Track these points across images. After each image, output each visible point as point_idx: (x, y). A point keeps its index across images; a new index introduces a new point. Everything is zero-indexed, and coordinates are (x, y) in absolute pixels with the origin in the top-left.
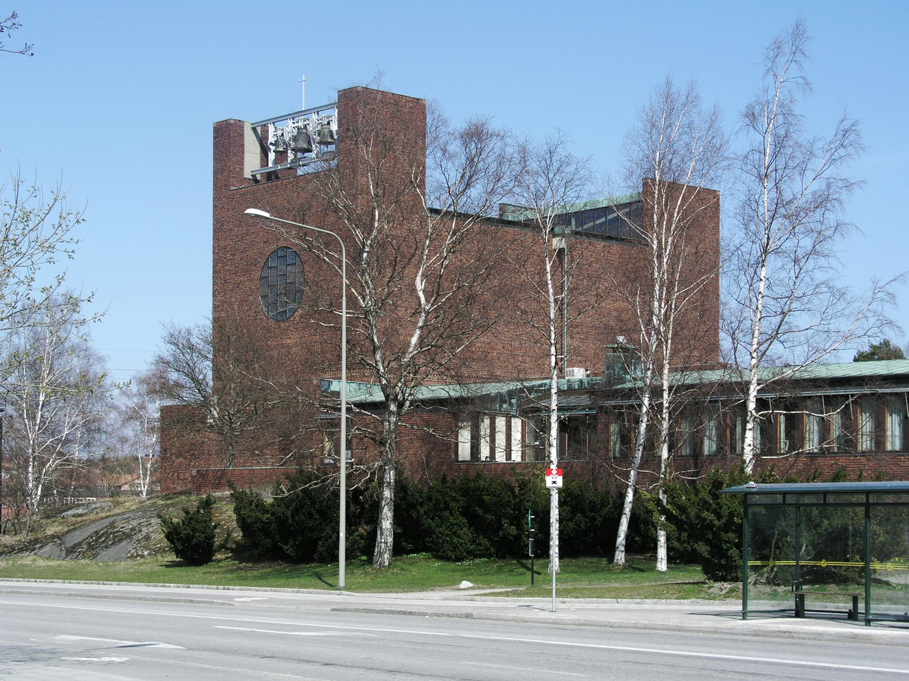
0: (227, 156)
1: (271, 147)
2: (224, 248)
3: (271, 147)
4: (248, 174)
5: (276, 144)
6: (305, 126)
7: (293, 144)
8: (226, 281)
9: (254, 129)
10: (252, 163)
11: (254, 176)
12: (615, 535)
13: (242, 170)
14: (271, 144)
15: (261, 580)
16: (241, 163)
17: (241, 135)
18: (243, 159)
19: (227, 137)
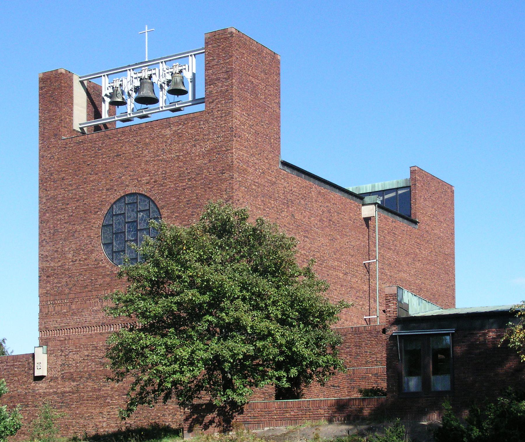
0: (57, 105)
1: (106, 98)
2: (54, 198)
3: (106, 98)
4: (76, 127)
5: (111, 96)
6: (150, 77)
7: (134, 95)
8: (56, 231)
9: (82, 82)
10: (80, 116)
11: (82, 129)
12: (433, 364)
13: (71, 121)
14: (106, 95)
15: (500, 309)
16: (71, 114)
17: (71, 87)
18: (72, 110)
19: (54, 89)
